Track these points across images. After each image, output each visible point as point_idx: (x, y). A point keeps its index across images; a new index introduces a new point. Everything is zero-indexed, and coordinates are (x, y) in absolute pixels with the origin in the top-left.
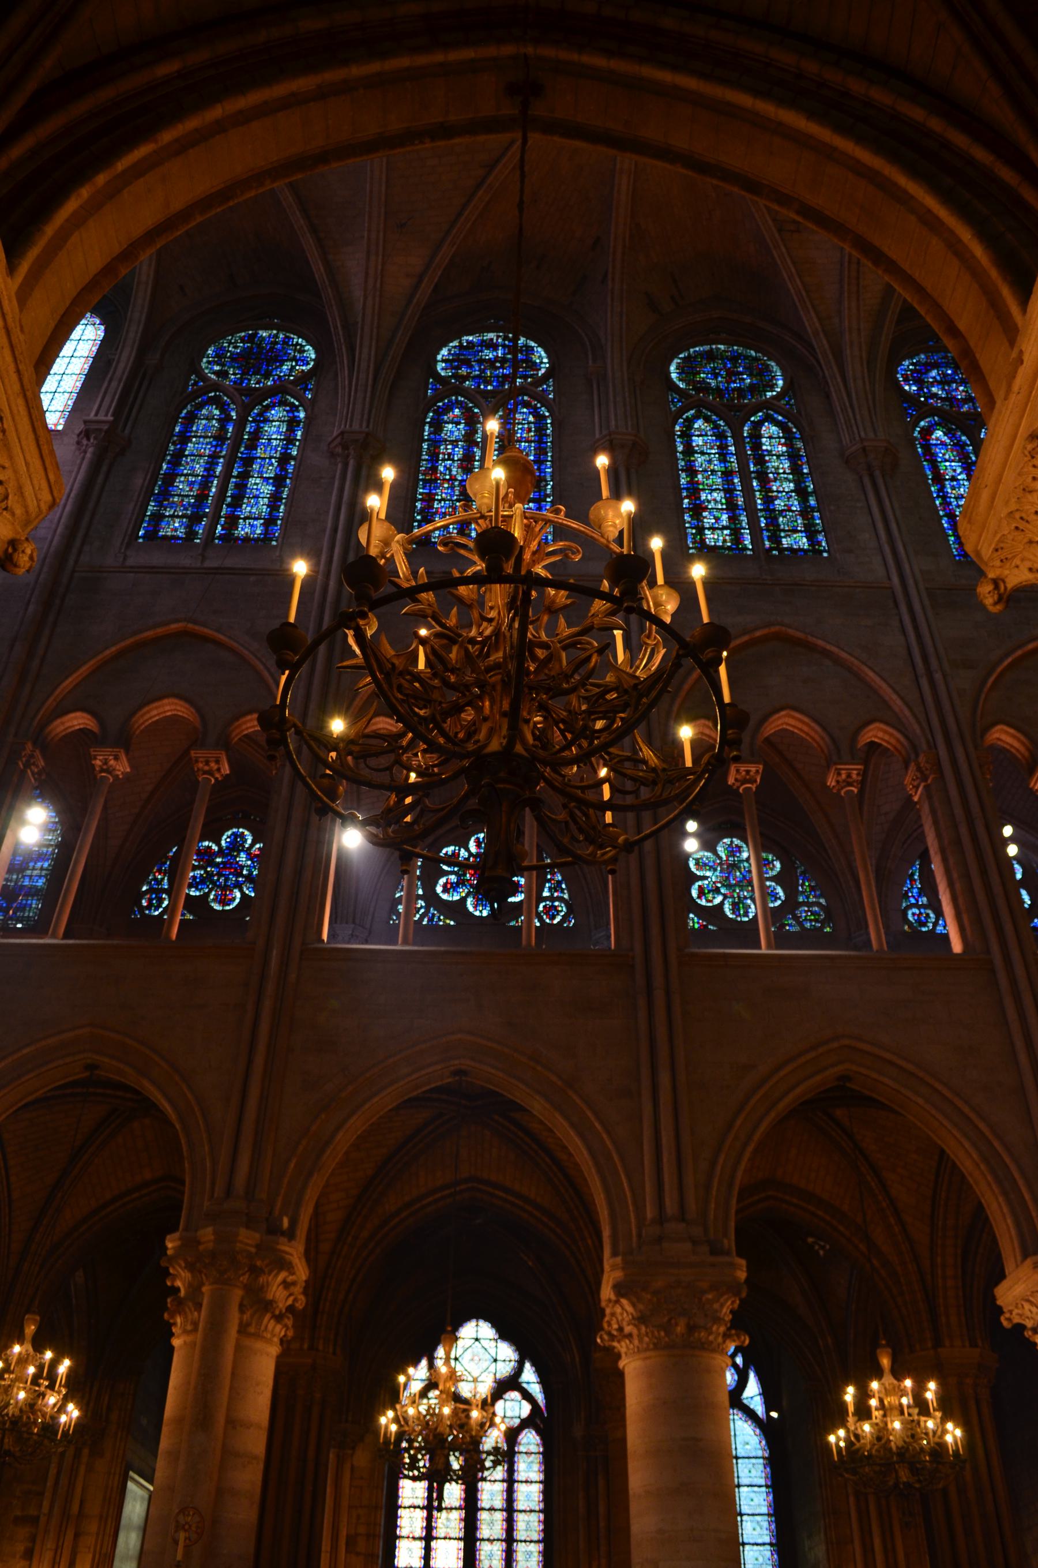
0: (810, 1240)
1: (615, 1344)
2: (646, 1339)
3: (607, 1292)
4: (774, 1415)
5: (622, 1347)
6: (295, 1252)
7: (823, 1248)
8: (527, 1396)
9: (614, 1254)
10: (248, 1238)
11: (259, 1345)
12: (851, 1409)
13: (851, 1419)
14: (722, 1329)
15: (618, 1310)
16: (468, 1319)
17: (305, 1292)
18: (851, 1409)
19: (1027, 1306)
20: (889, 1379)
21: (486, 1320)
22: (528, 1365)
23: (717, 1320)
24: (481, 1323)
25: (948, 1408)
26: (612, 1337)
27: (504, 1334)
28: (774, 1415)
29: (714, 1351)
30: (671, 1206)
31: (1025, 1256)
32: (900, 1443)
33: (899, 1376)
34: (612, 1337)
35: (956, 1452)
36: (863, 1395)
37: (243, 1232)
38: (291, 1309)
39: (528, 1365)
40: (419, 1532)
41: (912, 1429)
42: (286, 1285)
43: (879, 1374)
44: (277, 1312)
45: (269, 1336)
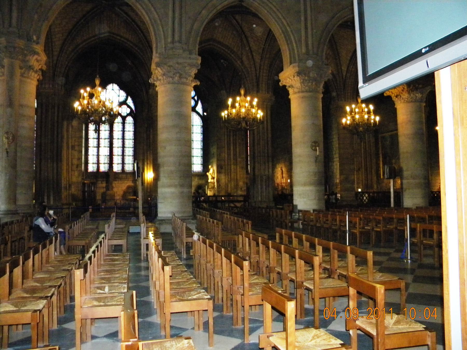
0: (222, 61)
1: (155, 83)
2: (165, 81)
3: (153, 66)
4: (205, 114)
5: (157, 83)
6: (39, 48)
7: (226, 64)
8: (129, 106)
9: (156, 53)
10: (21, 43)
11: (29, 80)
12: (230, 106)
13: (229, 108)
14: (191, 79)
15: (157, 71)
16: (110, 83)
17: (46, 64)
18: (230, 106)
19: (288, 79)
20: (243, 97)
21: (116, 84)
22: (129, 98)
23: (190, 76)
24: (114, 85)
25: (260, 106)
26: (154, 81)
27: (122, 88)
28: (205, 114)
29: (188, 85)
30: (177, 38)
31: (291, 63)
32: (244, 116)
33: (245, 95)
34: (154, 81)
35: (260, 120)
36: (234, 102)
37: (18, 40)
38: (41, 70)
39: (129, 98)
40: (95, 145)
41: (248, 110)
42: (37, 61)
43: (240, 95)
44: (35, 69)
45: (33, 78)
